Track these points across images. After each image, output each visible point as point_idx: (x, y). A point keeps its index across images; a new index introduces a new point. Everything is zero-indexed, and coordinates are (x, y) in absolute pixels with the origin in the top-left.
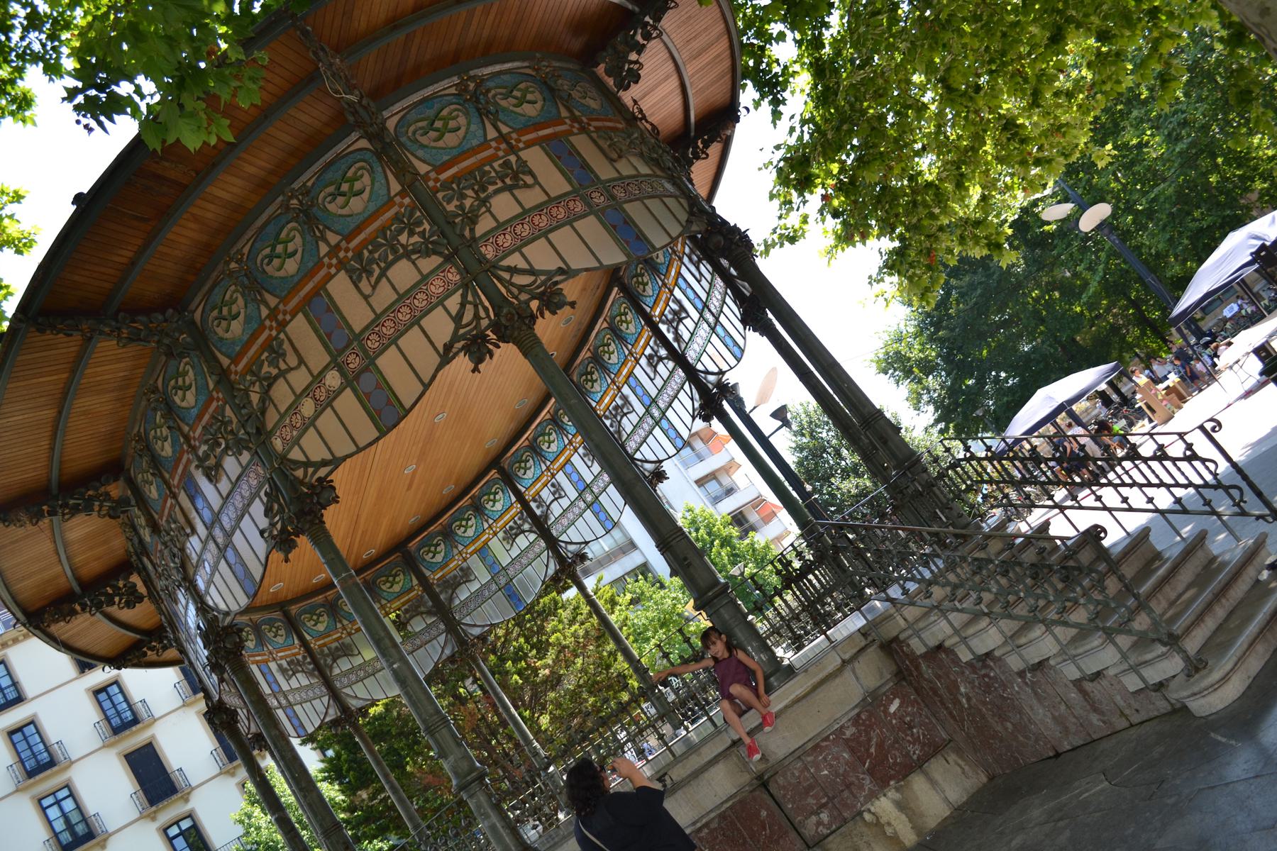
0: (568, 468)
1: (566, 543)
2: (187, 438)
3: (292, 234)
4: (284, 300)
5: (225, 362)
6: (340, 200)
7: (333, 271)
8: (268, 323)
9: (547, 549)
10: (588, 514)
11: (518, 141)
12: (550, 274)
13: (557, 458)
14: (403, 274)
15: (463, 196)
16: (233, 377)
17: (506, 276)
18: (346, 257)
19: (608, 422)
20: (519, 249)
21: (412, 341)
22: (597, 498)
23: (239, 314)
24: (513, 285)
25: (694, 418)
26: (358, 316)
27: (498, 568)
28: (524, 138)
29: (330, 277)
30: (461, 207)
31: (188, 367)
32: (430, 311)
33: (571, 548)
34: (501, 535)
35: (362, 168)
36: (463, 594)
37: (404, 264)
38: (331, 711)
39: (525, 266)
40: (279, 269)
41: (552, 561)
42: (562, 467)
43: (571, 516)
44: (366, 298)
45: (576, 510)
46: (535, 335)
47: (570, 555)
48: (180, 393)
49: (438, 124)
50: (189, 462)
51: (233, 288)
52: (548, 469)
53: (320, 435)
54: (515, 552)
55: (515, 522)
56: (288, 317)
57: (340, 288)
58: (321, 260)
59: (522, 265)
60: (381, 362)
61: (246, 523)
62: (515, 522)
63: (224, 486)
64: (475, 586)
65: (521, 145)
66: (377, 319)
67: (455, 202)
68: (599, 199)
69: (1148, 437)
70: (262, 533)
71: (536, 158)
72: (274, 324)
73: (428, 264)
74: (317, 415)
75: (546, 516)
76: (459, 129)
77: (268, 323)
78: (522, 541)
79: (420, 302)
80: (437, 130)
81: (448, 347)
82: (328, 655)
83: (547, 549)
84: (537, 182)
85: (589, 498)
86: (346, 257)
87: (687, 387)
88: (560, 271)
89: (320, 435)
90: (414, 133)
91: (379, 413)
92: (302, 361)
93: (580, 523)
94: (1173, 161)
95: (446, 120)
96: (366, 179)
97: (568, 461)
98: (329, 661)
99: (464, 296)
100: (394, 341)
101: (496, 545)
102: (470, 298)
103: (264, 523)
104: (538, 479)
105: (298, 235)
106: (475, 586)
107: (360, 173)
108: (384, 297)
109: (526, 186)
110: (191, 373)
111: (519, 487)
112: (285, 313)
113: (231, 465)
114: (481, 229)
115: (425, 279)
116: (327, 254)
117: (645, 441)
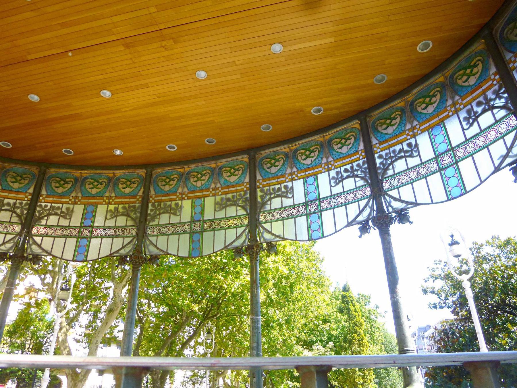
3: (315, 150)
9: (247, 226)
18: (152, 201)
19: (150, 207)
21: (340, 211)
32: (352, 203)
34: (218, 198)
35: (353, 135)
40: (268, 168)
41: (243, 237)
46: (388, 230)
53: (347, 218)
54: (221, 214)
55: (352, 167)
60: (93, 241)
69: (396, 362)
74: (173, 234)
75: (264, 204)
78: (232, 211)
79: (351, 197)
83: (247, 226)
86: (152, 201)
89: (347, 218)
91: (199, 241)
96: (136, 185)
100: (102, 237)
115: (43, 236)
116: (324, 163)
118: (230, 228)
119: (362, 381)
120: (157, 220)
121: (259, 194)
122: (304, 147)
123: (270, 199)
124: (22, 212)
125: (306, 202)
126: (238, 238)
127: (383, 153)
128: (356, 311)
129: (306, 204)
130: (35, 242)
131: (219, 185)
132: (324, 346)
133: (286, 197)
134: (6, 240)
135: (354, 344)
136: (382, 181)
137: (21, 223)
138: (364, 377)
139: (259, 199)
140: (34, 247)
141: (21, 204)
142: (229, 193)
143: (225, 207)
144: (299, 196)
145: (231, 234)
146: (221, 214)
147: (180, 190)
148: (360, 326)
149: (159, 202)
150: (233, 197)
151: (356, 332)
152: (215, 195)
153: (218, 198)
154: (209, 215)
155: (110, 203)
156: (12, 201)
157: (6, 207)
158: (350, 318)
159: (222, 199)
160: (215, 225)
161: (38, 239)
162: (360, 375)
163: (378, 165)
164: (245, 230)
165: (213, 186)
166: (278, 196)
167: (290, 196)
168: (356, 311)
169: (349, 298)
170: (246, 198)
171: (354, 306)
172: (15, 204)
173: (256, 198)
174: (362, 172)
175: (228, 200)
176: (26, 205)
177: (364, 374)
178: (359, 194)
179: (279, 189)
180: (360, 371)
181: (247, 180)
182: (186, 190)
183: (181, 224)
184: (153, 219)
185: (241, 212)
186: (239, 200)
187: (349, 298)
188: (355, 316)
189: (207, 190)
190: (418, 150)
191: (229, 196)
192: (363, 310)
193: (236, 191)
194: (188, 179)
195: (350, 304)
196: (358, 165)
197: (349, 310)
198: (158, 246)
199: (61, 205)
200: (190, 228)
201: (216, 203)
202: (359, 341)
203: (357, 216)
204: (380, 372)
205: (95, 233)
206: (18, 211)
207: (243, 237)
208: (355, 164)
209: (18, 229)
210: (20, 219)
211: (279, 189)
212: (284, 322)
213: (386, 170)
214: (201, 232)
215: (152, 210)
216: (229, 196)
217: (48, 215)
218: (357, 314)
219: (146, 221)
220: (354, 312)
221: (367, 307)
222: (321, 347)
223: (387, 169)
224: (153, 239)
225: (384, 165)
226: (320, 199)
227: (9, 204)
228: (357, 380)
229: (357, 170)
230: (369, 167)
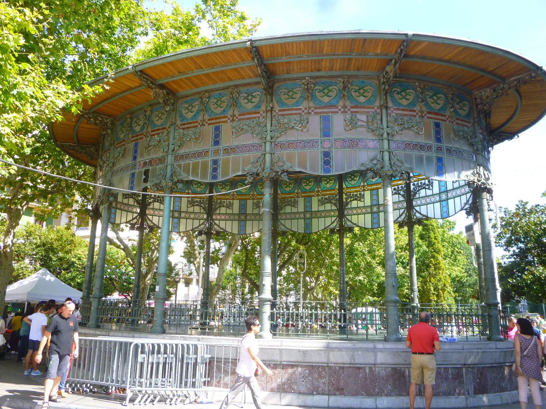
0: (374, 192)
1: (417, 211)
6: (358, 94)
9: (337, 217)
10: (437, 205)
13: (372, 185)
19: (279, 201)
20: (153, 216)
22: (379, 212)
25: (462, 209)
27: (308, 209)
33: (349, 223)
34: (320, 198)
36: (288, 209)
39: (218, 224)
41: (336, 223)
42: (372, 190)
43: (428, 200)
45: (433, 199)
47: (415, 217)
49: (362, 91)
52: (364, 186)
54: (322, 208)
55: (398, 188)
62: (398, 188)
64: (294, 210)
66: (187, 212)
74: (294, 219)
75: (347, 204)
78: (328, 206)
83: (337, 217)
85: (375, 209)
87: (469, 195)
93: (430, 206)
95: (365, 91)
97: (377, 189)
101: (315, 200)
104: (355, 187)
106: (294, 210)
107: (369, 90)
108: (191, 210)
111: (344, 184)
112: (237, 118)
117: (454, 198)
118: (328, 217)
119: (436, 299)
120: (284, 210)
121: (344, 196)
122: (379, 122)
123: (351, 201)
124: (205, 206)
125: (371, 206)
126: (332, 223)
127: (416, 183)
128: (436, 239)
129: (371, 206)
130: (216, 224)
131: (320, 189)
132: (405, 268)
133: (360, 200)
134: (201, 223)
135: (431, 267)
136: (413, 200)
137: (206, 213)
138: (438, 296)
139: (344, 200)
140: (215, 226)
141: (203, 201)
142: (326, 195)
143: (324, 204)
144: (368, 201)
145: (328, 221)
146: (322, 208)
147: (296, 191)
148: (438, 252)
149: (284, 198)
150: (329, 197)
151: (434, 257)
152: (318, 195)
153: (320, 198)
154: (315, 208)
155: (254, 199)
156: (198, 200)
157: (196, 203)
158: (430, 245)
159: (322, 198)
160: (318, 215)
161: (217, 222)
162: (433, 294)
163: (412, 189)
164: (336, 219)
165: (316, 189)
166: (356, 199)
167: (363, 200)
168: (436, 239)
169: (431, 227)
170: (337, 199)
171: (434, 234)
172: (200, 201)
173: (343, 200)
174: (403, 192)
175: (326, 199)
176: (206, 201)
177: (439, 293)
178: (400, 205)
179: (356, 195)
180: (434, 291)
181: (337, 187)
182: (300, 191)
183: (298, 213)
184: (281, 209)
185: (334, 208)
186: (332, 199)
187: (431, 227)
188: (434, 243)
189: (313, 191)
190: (432, 186)
191: (327, 197)
192: (446, 235)
193: (330, 194)
194: (300, 183)
195: (431, 232)
196: (402, 187)
197: (429, 237)
198: (422, 213)
199: (226, 201)
200: (304, 216)
201: (319, 201)
202: (436, 264)
203: (398, 218)
204: (466, 291)
205: (248, 218)
206: (203, 205)
207: (336, 223)
208: (400, 186)
209: (205, 216)
210: (205, 210)
211: (356, 195)
212: (367, 252)
213: (416, 193)
214: (311, 218)
215: (280, 203)
216: (327, 197)
217: (220, 207)
218: (436, 241)
219: (277, 210)
220: (433, 239)
221: (451, 233)
222: (402, 269)
223: (416, 193)
224: (283, 222)
225: (415, 190)
226: (379, 205)
227: (197, 201)
228: (431, 298)
229: (401, 190)
230: (406, 190)
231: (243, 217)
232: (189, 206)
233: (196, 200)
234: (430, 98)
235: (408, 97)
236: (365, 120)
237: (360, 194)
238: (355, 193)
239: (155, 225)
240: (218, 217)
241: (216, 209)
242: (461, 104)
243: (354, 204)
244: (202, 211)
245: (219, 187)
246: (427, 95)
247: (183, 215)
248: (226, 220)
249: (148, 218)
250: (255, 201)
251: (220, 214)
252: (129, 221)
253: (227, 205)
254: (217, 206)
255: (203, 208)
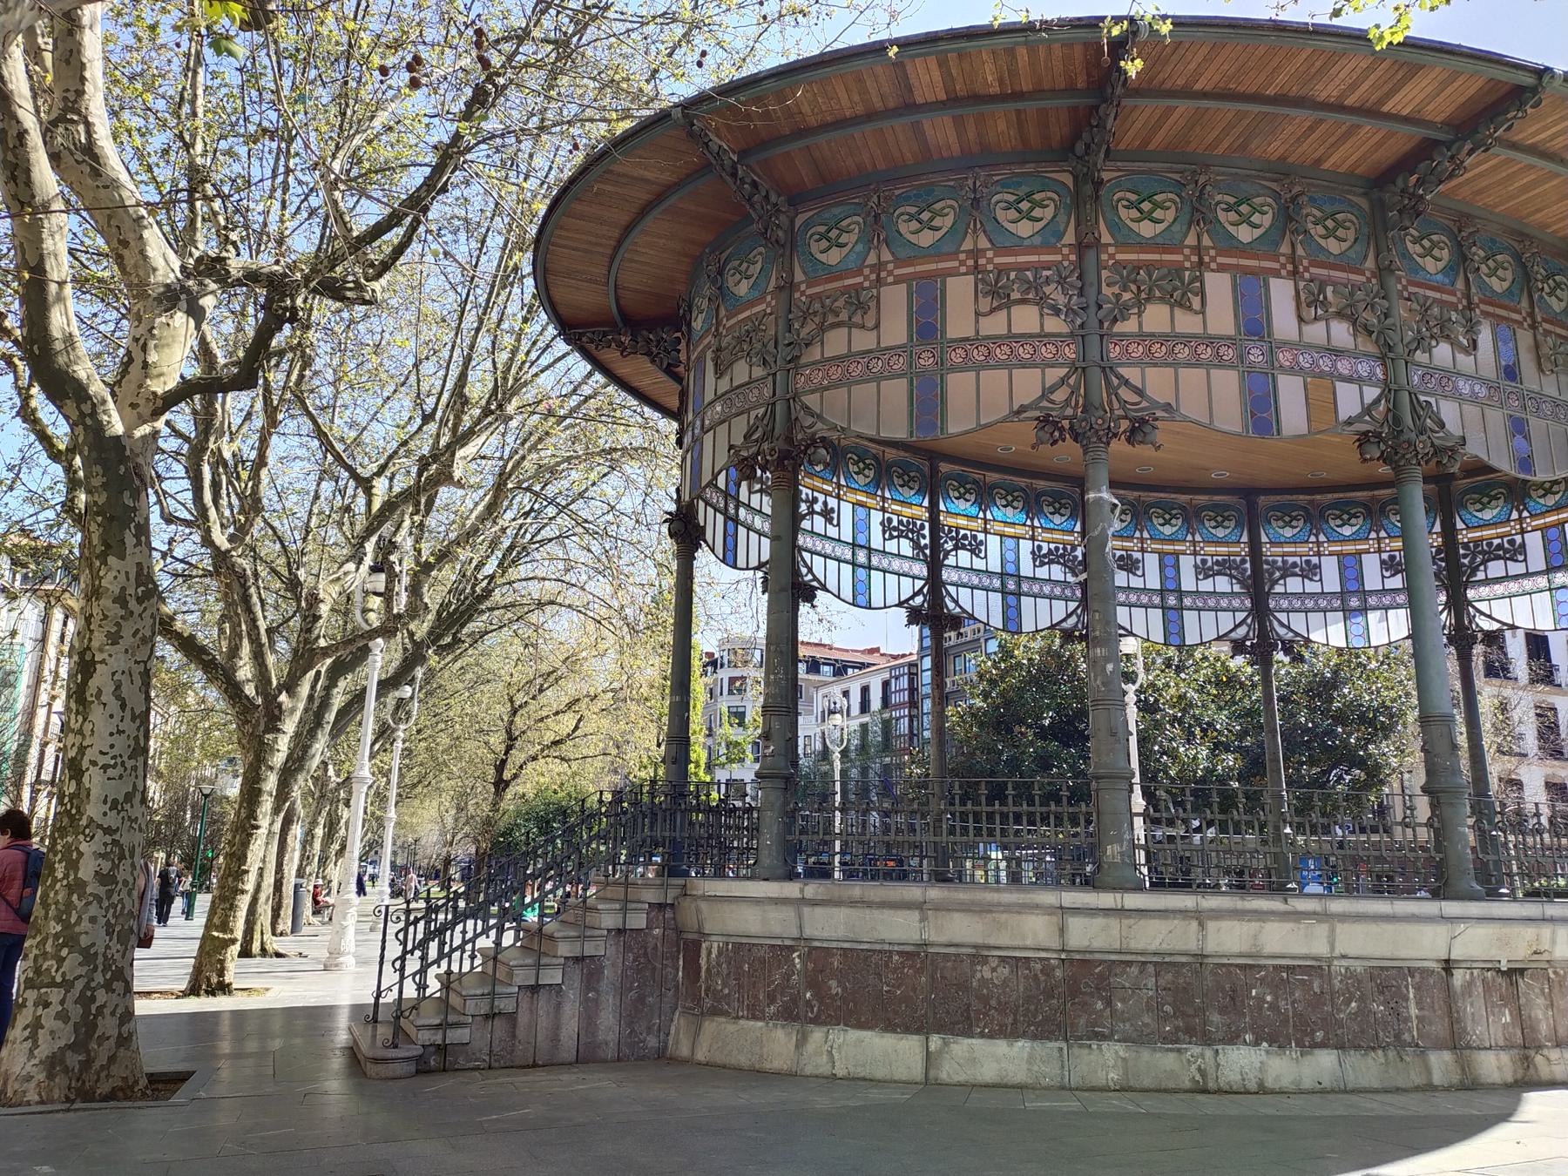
0: (1553, 533)
2: (718, 323)
4: (899, 262)
5: (799, 276)
7: (963, 269)
8: (867, 271)
11: (1213, 259)
12: (1155, 404)
13: (1543, 514)
14: (1026, 319)
15: (1125, 289)
16: (797, 295)
17: (1115, 381)
23: (844, 245)
24: (1117, 395)
26: (959, 323)
28: (1220, 260)
29: (954, 273)
30: (1118, 296)
31: (759, 258)
37: (1033, 311)
38: (919, 600)
42: (1543, 529)
44: (977, 314)
48: (738, 276)
50: (708, 346)
51: (856, 218)
56: (890, 279)
57: (960, 291)
58: (957, 252)
59: (1136, 381)
61: (722, 430)
63: (724, 385)
65: (1214, 266)
66: (976, 340)
67: (1116, 290)
68: (1256, 356)
70: (731, 447)
71: (1218, 287)
72: (873, 277)
73: (1055, 325)
76: (1161, 221)
77: (867, 271)
80: (1140, 211)
81: (1023, 409)
82: (952, 539)
83: (1268, 594)
84: (1203, 312)
88: (1167, 407)
90: (1119, 200)
92: (877, 326)
94: (381, 364)
98: (949, 546)
99: (1068, 376)
102: (1072, 381)
103: (738, 440)
105: (952, 216)
108: (994, 325)
109: (1190, 308)
110: (759, 266)
112: (890, 273)
113: (741, 372)
114: (1120, 327)
123: (1484, 562)
134: (1070, 610)
167: (1521, 558)
211: (1500, 547)
231: (1354, 602)
232: (1387, 574)
233: (1291, 560)
234: (1227, 210)
235: (937, 222)
236: (1005, 312)
237: (1512, 542)
238: (1496, 542)
239: (964, 611)
240: (1285, 604)
241: (1276, 582)
242: (1426, 243)
243: (1294, 585)
244: (1237, 588)
245: (1332, 523)
246: (1219, 203)
247: (1187, 602)
248: (1131, 605)
249: (948, 593)
250: (1199, 558)
251: (1285, 594)
252: (907, 601)
253: (1302, 570)
254: (1277, 574)
255: (1239, 582)
